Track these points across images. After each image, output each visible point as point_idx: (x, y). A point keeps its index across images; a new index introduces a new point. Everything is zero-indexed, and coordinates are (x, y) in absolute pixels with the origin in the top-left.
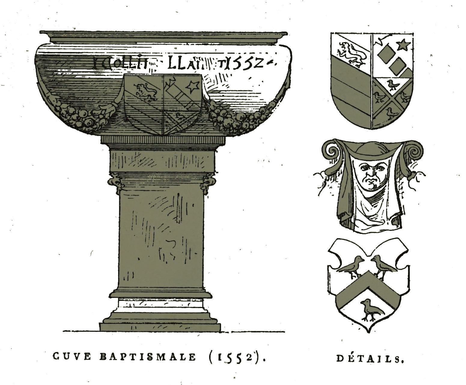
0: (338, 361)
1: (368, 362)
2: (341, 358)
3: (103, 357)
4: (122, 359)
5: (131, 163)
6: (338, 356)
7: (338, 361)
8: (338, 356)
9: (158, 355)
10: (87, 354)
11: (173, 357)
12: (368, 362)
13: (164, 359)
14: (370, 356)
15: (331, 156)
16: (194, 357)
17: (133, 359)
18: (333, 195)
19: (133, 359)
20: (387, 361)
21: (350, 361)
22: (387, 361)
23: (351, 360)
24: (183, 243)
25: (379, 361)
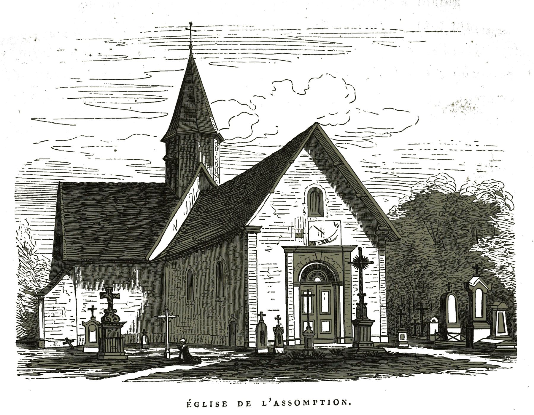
0: (239, 406)
1: (275, 406)
2: (240, 404)
3: (240, 404)
4: (314, 404)
5: (387, 39)
6: (239, 402)
7: (239, 406)
8: (239, 402)
9: (304, 401)
10: (248, 403)
11: (284, 403)
12: (275, 406)
13: (309, 404)
14: (276, 401)
15: (435, 316)
16: (250, 403)
17: (322, 404)
18: (277, 127)
19: (322, 404)
20: (204, 406)
21: (247, 406)
22: (204, 406)
23: (189, 406)
24: (141, 135)
25: (211, 406)
